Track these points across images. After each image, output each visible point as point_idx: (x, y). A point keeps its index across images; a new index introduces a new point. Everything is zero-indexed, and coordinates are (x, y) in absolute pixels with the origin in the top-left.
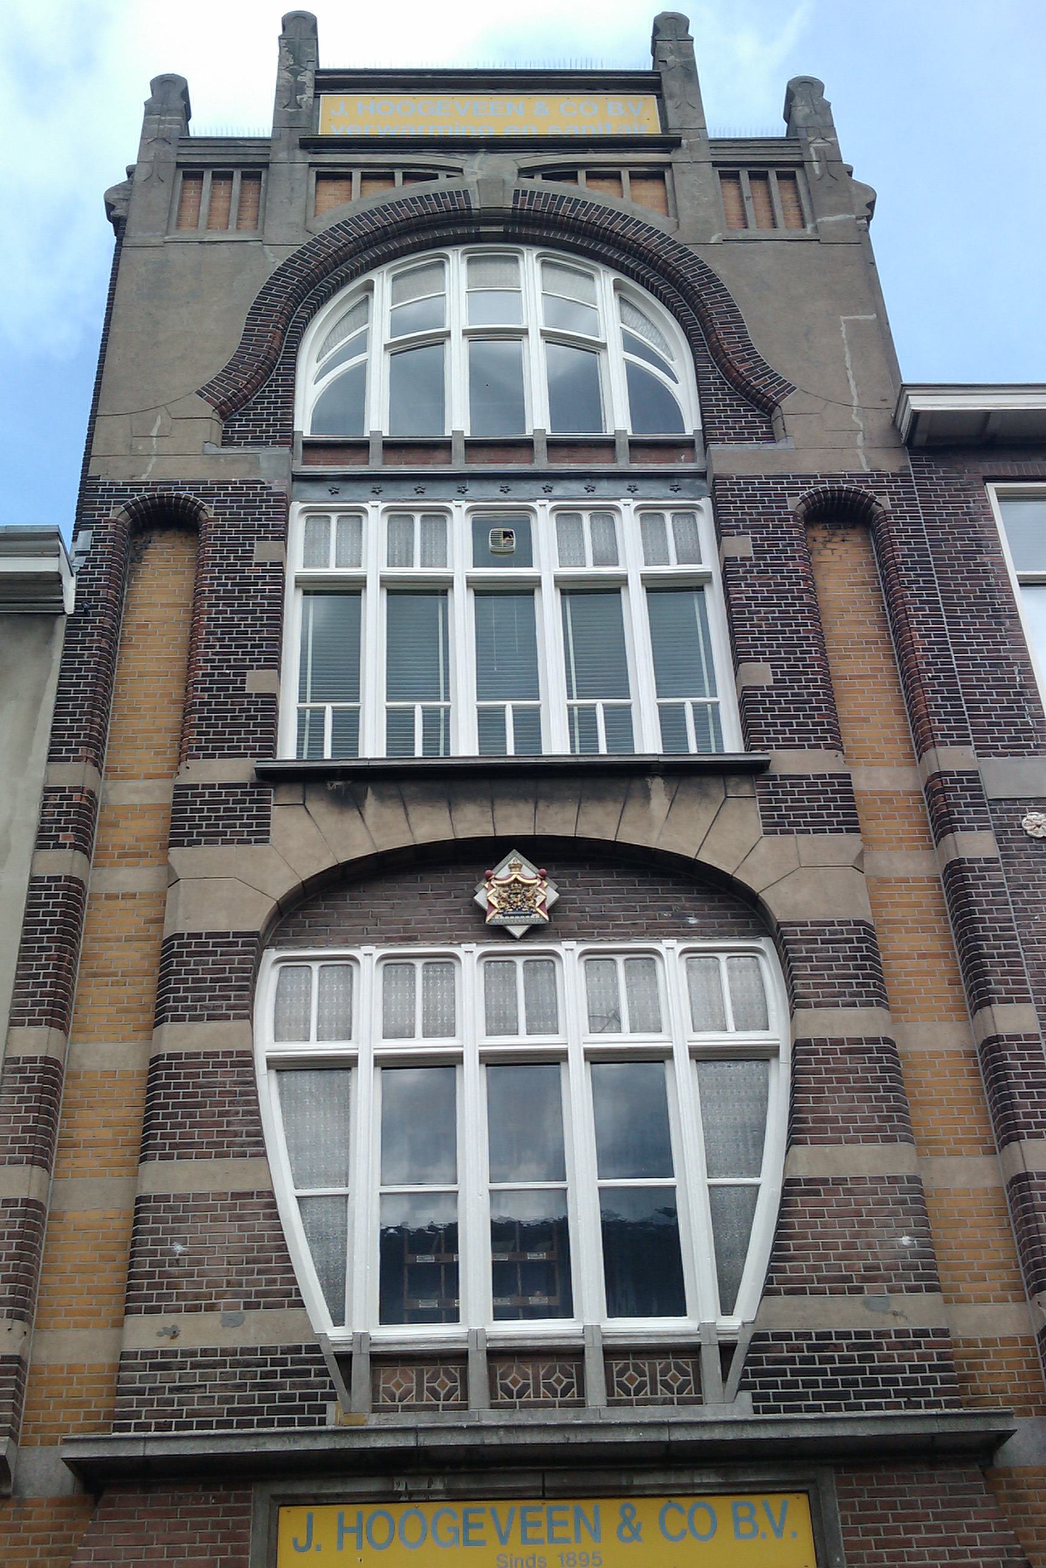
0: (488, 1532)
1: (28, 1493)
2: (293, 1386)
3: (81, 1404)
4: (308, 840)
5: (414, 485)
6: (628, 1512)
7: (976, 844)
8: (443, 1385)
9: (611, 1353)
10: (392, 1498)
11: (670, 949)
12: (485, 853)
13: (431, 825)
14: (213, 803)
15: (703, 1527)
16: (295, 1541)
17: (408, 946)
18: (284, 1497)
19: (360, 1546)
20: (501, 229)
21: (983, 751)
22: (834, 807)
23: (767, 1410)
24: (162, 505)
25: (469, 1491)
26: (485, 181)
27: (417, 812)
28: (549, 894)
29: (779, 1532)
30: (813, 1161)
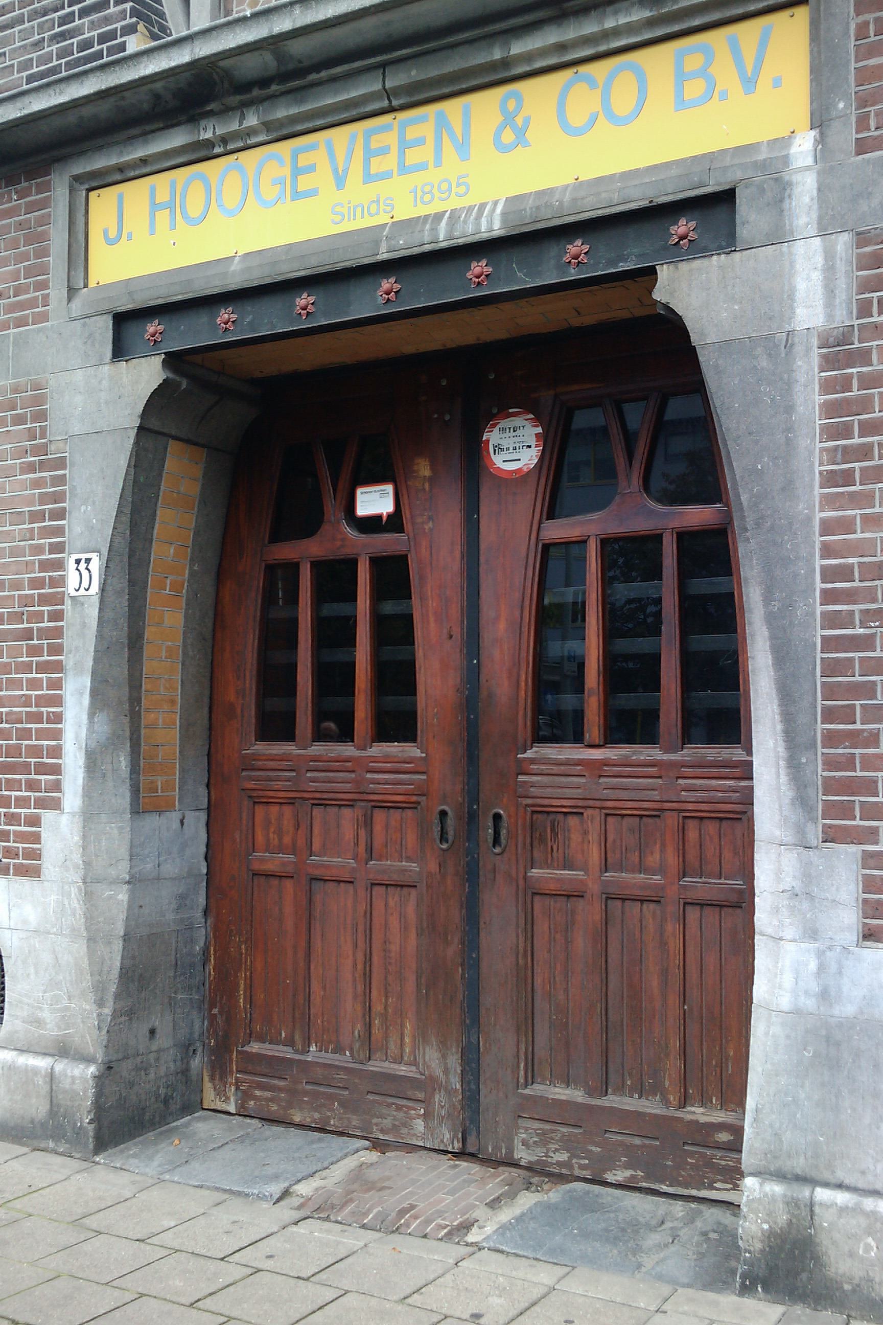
0: (322, 178)
6: (512, 105)
10: (202, 153)
16: (106, 232)
18: (93, 175)
19: (173, 227)
25: (293, 120)
29: (749, 83)
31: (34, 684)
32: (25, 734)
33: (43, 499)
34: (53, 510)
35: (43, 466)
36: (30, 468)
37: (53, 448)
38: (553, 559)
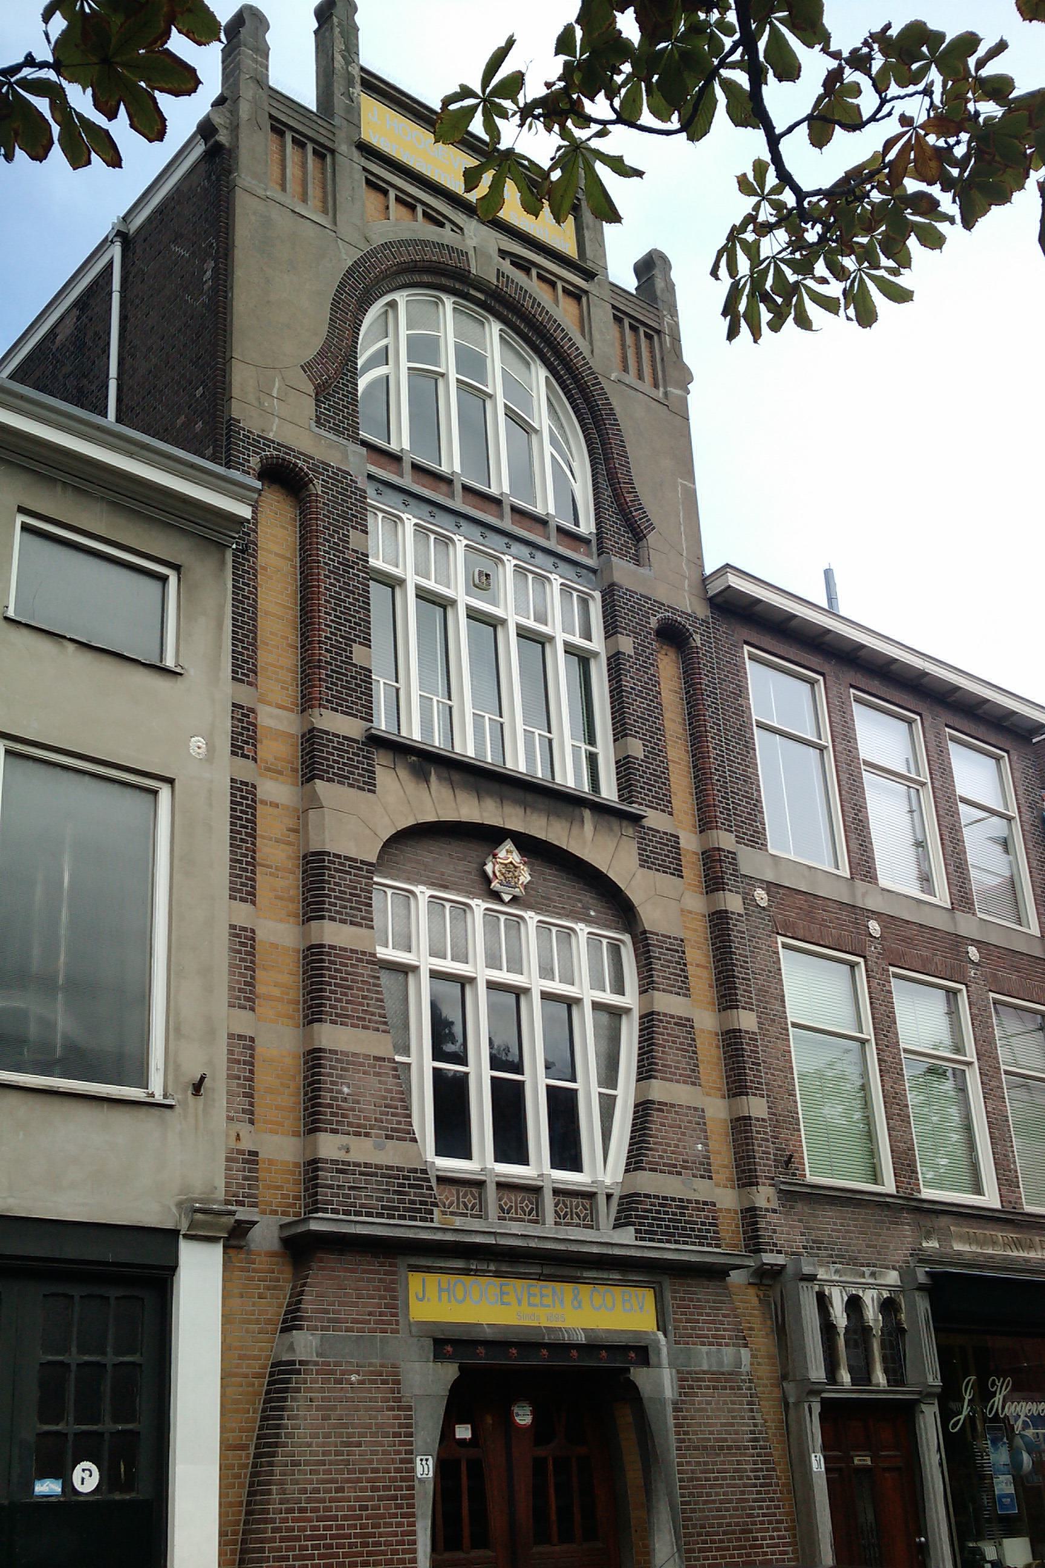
1: (253, 1246)
2: (415, 1195)
3: (278, 1188)
5: (430, 508)
8: (470, 1201)
9: (556, 1192)
10: (466, 1272)
11: (582, 930)
12: (490, 837)
13: (470, 809)
15: (460, 1294)
17: (444, 892)
19: (450, 1301)
20: (482, 297)
21: (739, 840)
23: (642, 1239)
24: (282, 465)
27: (462, 795)
28: (525, 877)
31: (399, 1525)
32: (395, 1552)
33: (400, 1426)
34: (406, 1432)
35: (399, 1408)
36: (392, 1409)
37: (404, 1399)
38: (539, 1466)
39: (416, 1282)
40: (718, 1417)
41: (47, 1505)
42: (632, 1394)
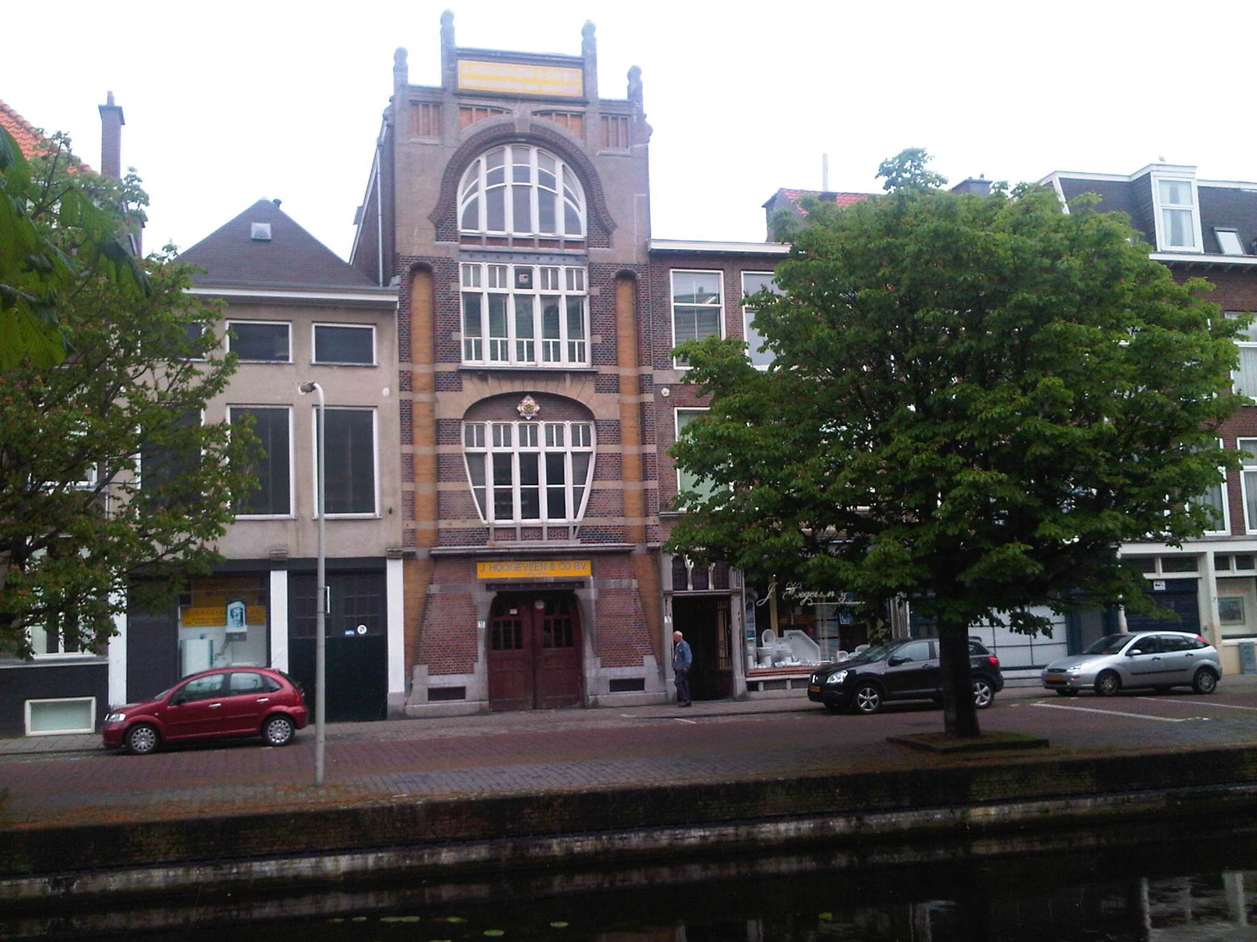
4: (473, 392)
7: (649, 398)
11: (568, 425)
12: (522, 395)
13: (507, 388)
14: (446, 378)
22: (612, 385)
26: (519, 115)
27: (503, 383)
30: (599, 485)
39: (480, 566)
40: (615, 604)
41: (350, 637)
42: (575, 599)
